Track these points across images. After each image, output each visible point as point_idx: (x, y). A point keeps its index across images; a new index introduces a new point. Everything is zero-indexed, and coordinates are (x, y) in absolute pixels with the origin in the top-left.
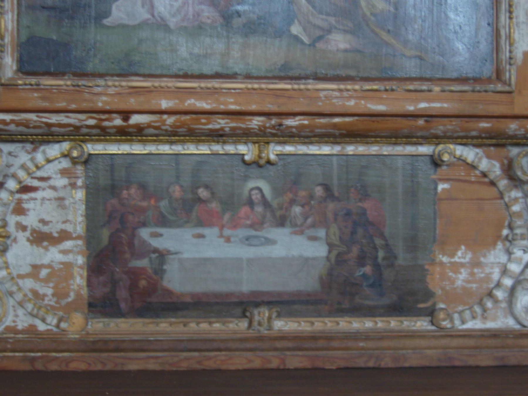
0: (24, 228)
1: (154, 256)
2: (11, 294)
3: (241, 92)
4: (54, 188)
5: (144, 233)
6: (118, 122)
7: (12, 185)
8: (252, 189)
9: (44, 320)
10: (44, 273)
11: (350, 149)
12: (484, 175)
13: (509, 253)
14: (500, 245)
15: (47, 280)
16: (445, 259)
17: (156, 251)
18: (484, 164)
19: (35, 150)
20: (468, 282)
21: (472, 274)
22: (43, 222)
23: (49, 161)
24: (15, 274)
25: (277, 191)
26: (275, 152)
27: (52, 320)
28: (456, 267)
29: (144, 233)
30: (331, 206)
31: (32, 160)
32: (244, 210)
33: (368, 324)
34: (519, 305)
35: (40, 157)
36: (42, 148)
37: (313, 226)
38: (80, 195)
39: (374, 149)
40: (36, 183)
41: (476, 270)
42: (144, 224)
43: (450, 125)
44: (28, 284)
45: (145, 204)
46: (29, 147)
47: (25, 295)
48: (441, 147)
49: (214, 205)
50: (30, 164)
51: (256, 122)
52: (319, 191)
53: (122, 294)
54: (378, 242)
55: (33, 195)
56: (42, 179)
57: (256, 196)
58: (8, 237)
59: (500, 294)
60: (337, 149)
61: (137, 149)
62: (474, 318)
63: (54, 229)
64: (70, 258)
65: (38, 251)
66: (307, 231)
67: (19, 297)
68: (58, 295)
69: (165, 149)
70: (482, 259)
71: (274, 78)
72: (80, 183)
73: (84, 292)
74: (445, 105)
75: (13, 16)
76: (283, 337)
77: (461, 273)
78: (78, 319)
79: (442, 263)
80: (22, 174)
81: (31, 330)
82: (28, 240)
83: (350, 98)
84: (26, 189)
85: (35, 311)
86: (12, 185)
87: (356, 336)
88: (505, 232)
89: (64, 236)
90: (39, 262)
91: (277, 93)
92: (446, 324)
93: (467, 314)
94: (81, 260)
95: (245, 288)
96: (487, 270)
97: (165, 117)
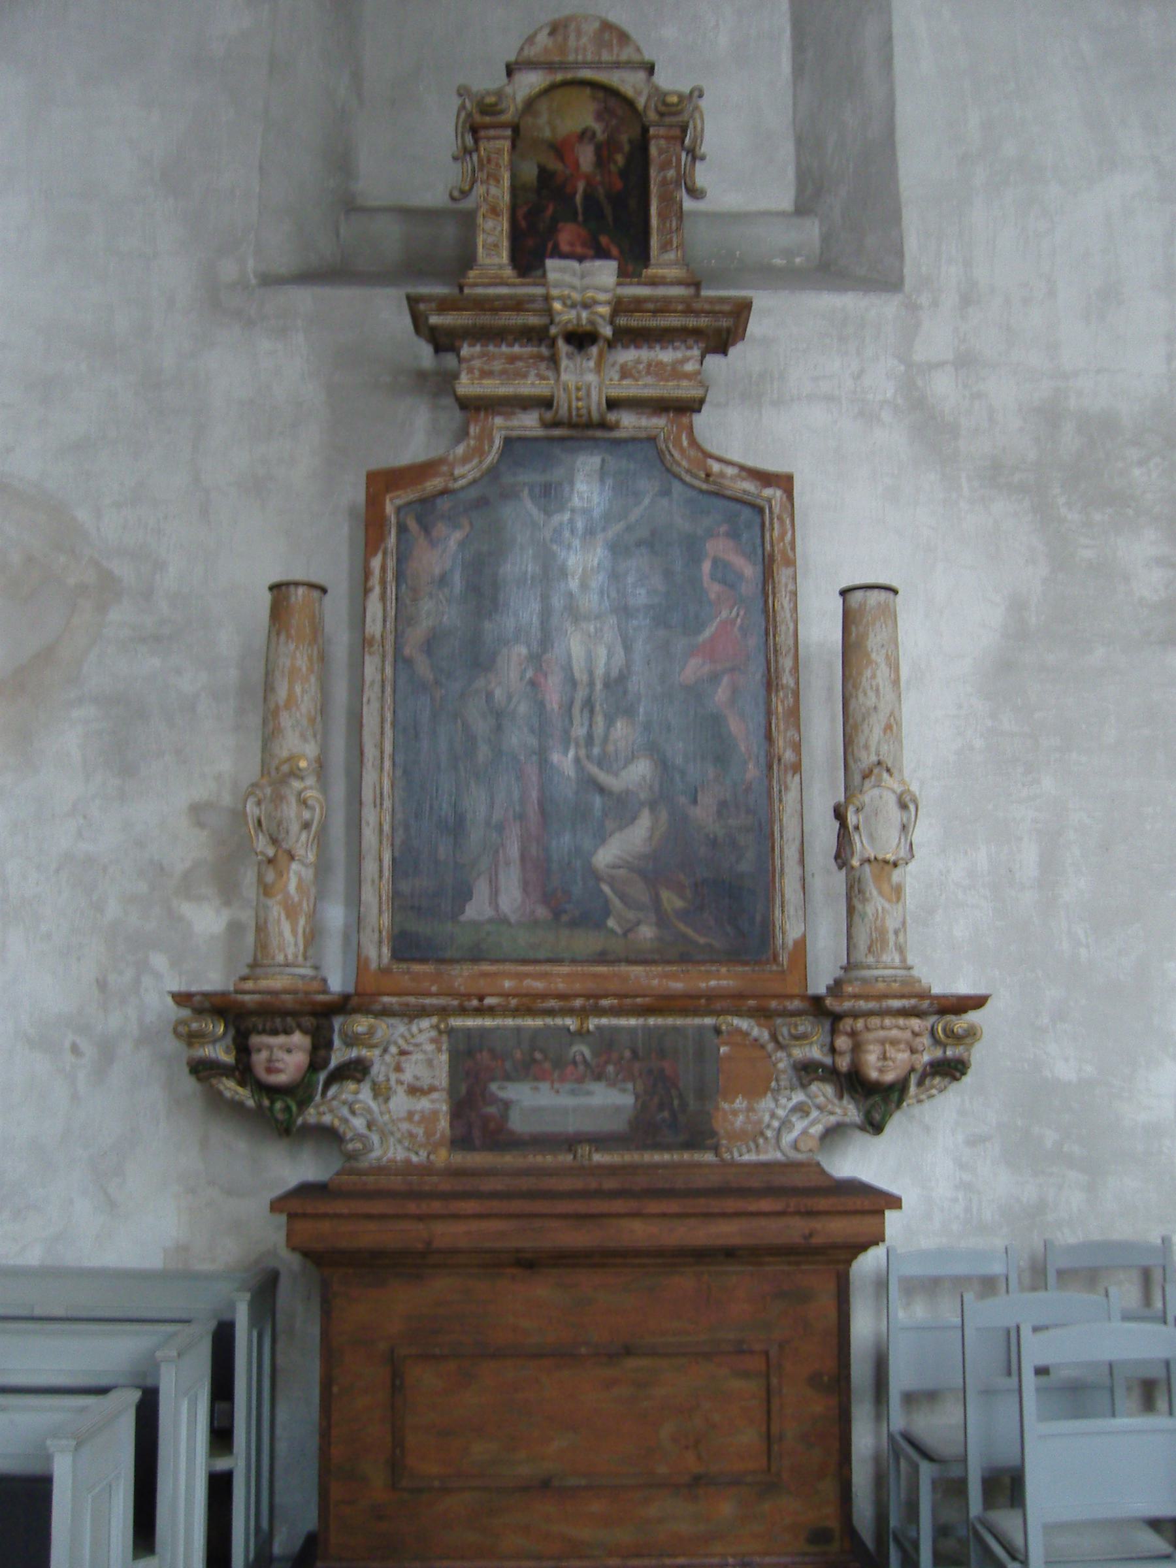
0: (400, 1082)
2: (392, 1133)
3: (568, 975)
5: (494, 1087)
6: (475, 1002)
7: (393, 1050)
8: (575, 1052)
9: (417, 1153)
11: (651, 1021)
12: (756, 1040)
13: (776, 1101)
14: (769, 1095)
15: (420, 1122)
17: (501, 1100)
18: (756, 1032)
19: (411, 1022)
21: (748, 1117)
22: (417, 1078)
24: (395, 1117)
25: (596, 1054)
27: (423, 1154)
29: (494, 1087)
30: (637, 1066)
31: (409, 1030)
32: (570, 1068)
33: (667, 1157)
34: (784, 1141)
35: (414, 1029)
36: (416, 1021)
37: (624, 1081)
38: (444, 1057)
39: (670, 1021)
40: (411, 1048)
41: (750, 1114)
42: (493, 1079)
43: (726, 1004)
44: (405, 1126)
46: (406, 1020)
47: (403, 1134)
48: (721, 1018)
49: (547, 1065)
50: (407, 1034)
51: (578, 1003)
52: (627, 1054)
53: (477, 1134)
54: (674, 1092)
56: (417, 1045)
57: (578, 1058)
58: (390, 1088)
59: (769, 1133)
60: (641, 1021)
61: (488, 1022)
62: (749, 1151)
63: (425, 1083)
64: (437, 1106)
67: (398, 1135)
68: (429, 1134)
69: (510, 1022)
72: (444, 1047)
73: (448, 1132)
74: (731, 982)
75: (388, 914)
76: (600, 1166)
78: (443, 1153)
79: (723, 1109)
80: (401, 1042)
81: (408, 1162)
83: (654, 978)
84: (403, 1053)
85: (411, 1146)
86: (393, 1050)
88: (773, 1084)
89: (432, 1089)
91: (595, 976)
92: (727, 1156)
93: (744, 1149)
94: (445, 1108)
95: (571, 1129)
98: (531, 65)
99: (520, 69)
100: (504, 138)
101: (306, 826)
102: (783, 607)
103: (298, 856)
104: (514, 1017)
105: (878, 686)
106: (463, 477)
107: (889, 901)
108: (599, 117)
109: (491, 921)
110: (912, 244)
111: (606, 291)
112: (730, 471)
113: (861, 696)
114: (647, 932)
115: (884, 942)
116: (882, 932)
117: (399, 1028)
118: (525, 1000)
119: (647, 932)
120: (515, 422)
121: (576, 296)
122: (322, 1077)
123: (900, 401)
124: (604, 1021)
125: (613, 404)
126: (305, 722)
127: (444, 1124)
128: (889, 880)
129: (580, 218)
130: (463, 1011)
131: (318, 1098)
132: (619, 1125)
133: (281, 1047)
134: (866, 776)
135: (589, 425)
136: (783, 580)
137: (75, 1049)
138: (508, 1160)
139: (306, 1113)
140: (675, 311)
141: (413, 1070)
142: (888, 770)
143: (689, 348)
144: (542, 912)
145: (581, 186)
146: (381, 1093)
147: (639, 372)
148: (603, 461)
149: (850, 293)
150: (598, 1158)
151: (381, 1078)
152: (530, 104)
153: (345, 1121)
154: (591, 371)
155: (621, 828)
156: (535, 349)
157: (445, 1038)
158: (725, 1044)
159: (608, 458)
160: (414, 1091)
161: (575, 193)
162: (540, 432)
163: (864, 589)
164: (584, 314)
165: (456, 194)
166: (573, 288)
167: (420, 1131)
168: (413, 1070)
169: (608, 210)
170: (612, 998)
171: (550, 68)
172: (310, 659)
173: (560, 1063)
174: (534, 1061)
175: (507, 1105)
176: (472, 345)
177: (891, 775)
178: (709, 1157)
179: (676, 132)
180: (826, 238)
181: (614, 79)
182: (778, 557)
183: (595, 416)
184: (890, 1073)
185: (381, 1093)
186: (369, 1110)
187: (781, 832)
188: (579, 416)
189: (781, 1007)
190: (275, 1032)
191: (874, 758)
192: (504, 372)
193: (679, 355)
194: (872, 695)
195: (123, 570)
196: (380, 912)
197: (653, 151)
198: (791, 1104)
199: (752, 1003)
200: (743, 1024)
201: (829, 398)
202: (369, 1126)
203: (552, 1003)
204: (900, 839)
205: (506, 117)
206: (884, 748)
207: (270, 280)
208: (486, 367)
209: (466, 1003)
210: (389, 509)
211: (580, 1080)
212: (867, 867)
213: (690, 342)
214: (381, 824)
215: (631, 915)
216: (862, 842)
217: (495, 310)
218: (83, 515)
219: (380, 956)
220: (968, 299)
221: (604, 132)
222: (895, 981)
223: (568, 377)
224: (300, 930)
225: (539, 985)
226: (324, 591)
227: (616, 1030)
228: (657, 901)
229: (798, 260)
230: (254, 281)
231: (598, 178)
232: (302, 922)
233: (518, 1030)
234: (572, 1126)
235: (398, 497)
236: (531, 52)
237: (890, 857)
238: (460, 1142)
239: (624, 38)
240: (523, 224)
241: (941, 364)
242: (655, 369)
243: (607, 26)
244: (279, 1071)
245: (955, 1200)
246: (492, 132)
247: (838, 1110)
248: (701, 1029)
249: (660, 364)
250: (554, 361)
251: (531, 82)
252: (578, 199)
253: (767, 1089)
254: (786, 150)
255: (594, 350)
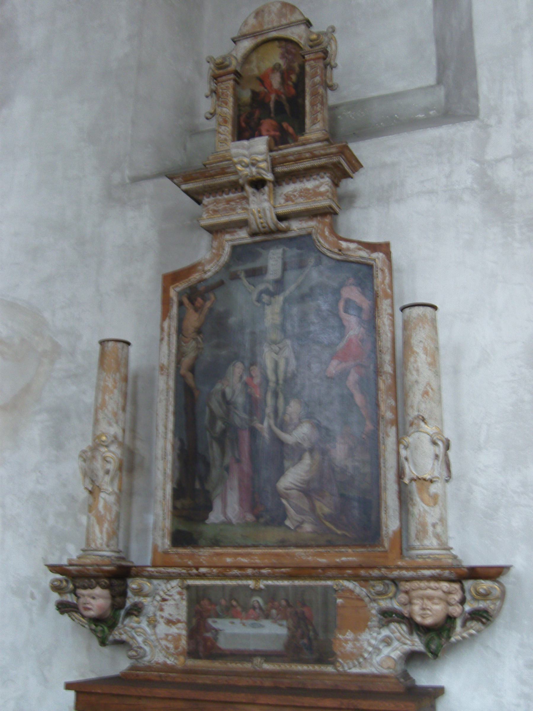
0: (162, 617)
1: (213, 631)
3: (263, 555)
4: (174, 600)
5: (210, 621)
6: (194, 571)
7: (158, 598)
10: (170, 637)
11: (297, 583)
16: (341, 637)
17: (214, 629)
20: (353, 648)
21: (354, 645)
22: (171, 615)
23: (172, 588)
25: (266, 603)
26: (263, 584)
28: (346, 641)
29: (210, 621)
30: (289, 610)
32: (251, 611)
35: (169, 586)
37: (282, 619)
38: (184, 603)
39: (307, 583)
40: (167, 597)
41: (356, 642)
42: (209, 617)
45: (210, 607)
46: (165, 581)
49: (239, 609)
52: (283, 603)
53: (201, 648)
54: (310, 627)
55: (166, 602)
57: (256, 605)
62: (355, 666)
63: (174, 619)
65: (168, 627)
66: (278, 621)
68: (176, 648)
69: (218, 582)
70: (359, 637)
71: (275, 546)
72: (184, 597)
73: (186, 647)
77: (348, 644)
78: (182, 658)
79: (340, 639)
80: (162, 593)
81: (165, 664)
82: (165, 623)
84: (164, 600)
87: (297, 673)
89: (179, 621)
90: (168, 633)
91: (277, 555)
92: (340, 669)
93: (351, 665)
94: (184, 632)
96: (361, 643)
97: (212, 569)
98: (244, 36)
99: (239, 40)
100: (230, 80)
101: (107, 472)
102: (384, 324)
103: (103, 489)
104: (221, 579)
105: (418, 366)
106: (209, 271)
107: (427, 505)
108: (283, 56)
109: (223, 523)
110: (484, 88)
111: (261, 154)
112: (352, 246)
113: (408, 374)
114: (308, 527)
115: (425, 532)
116: (424, 525)
117: (162, 586)
118: (220, 569)
119: (308, 527)
120: (236, 236)
121: (246, 160)
122: (123, 612)
123: (475, 186)
124: (270, 582)
125: (281, 218)
126: (110, 415)
127: (184, 642)
128: (428, 492)
129: (272, 115)
130: (191, 576)
131: (120, 625)
132: (278, 646)
133: (89, 596)
134: (411, 424)
135: (271, 232)
136: (384, 307)
137: (33, 597)
138: (217, 665)
139: (113, 633)
140: (307, 158)
141: (169, 610)
142: (423, 420)
143: (322, 178)
144: (250, 517)
145: (273, 97)
146: (153, 623)
147: (295, 196)
148: (284, 250)
149: (443, 126)
150: (267, 666)
151: (151, 614)
152: (247, 58)
153: (133, 638)
154: (266, 200)
155: (293, 465)
156: (240, 194)
157: (185, 592)
158: (340, 597)
159: (287, 249)
160: (170, 622)
161: (269, 102)
162: (249, 240)
163: (409, 308)
164: (254, 169)
165: (209, 116)
166: (245, 156)
167: (171, 646)
168: (169, 610)
169: (287, 108)
170: (267, 568)
171: (254, 36)
172: (115, 381)
173: (245, 609)
174: (232, 606)
175: (217, 631)
176: (208, 197)
177: (426, 423)
178: (330, 669)
179: (321, 55)
180: (448, 96)
181: (288, 33)
182: (381, 293)
183: (272, 226)
184: (428, 619)
185: (153, 623)
186: (145, 633)
187: (384, 463)
188: (264, 227)
189: (367, 574)
190: (85, 588)
191: (416, 413)
192: (225, 209)
193: (317, 183)
194: (414, 373)
195: (63, 342)
196: (164, 519)
197: (308, 68)
198: (380, 637)
199: (349, 571)
200: (346, 583)
201: (431, 192)
202: (145, 642)
203: (236, 572)
204: (433, 464)
205: (231, 68)
206: (423, 406)
207: (136, 180)
208: (216, 208)
209: (190, 572)
210: (173, 294)
211: (257, 618)
212: (414, 484)
213: (322, 174)
214: (165, 470)
215: (299, 518)
216: (409, 467)
217: (212, 176)
218: (47, 315)
219: (163, 544)
220: (520, 116)
221: (285, 64)
222: (429, 558)
223: (254, 207)
224: (104, 530)
225: (245, 561)
226: (128, 344)
227: (277, 587)
228: (313, 509)
229: (431, 113)
230: (128, 181)
231: (282, 91)
232: (106, 525)
233: (223, 587)
234: (252, 646)
235: (177, 286)
236: (246, 30)
237: (428, 477)
238: (192, 654)
239: (293, 8)
240: (243, 124)
241: (504, 159)
242: (306, 194)
243: (285, 5)
244: (89, 609)
245: (518, 705)
246: (224, 78)
247: (409, 642)
248: (326, 587)
249: (308, 190)
250: (246, 198)
251: (247, 44)
252: (272, 105)
253: (366, 626)
254: (431, 49)
255: (266, 189)
